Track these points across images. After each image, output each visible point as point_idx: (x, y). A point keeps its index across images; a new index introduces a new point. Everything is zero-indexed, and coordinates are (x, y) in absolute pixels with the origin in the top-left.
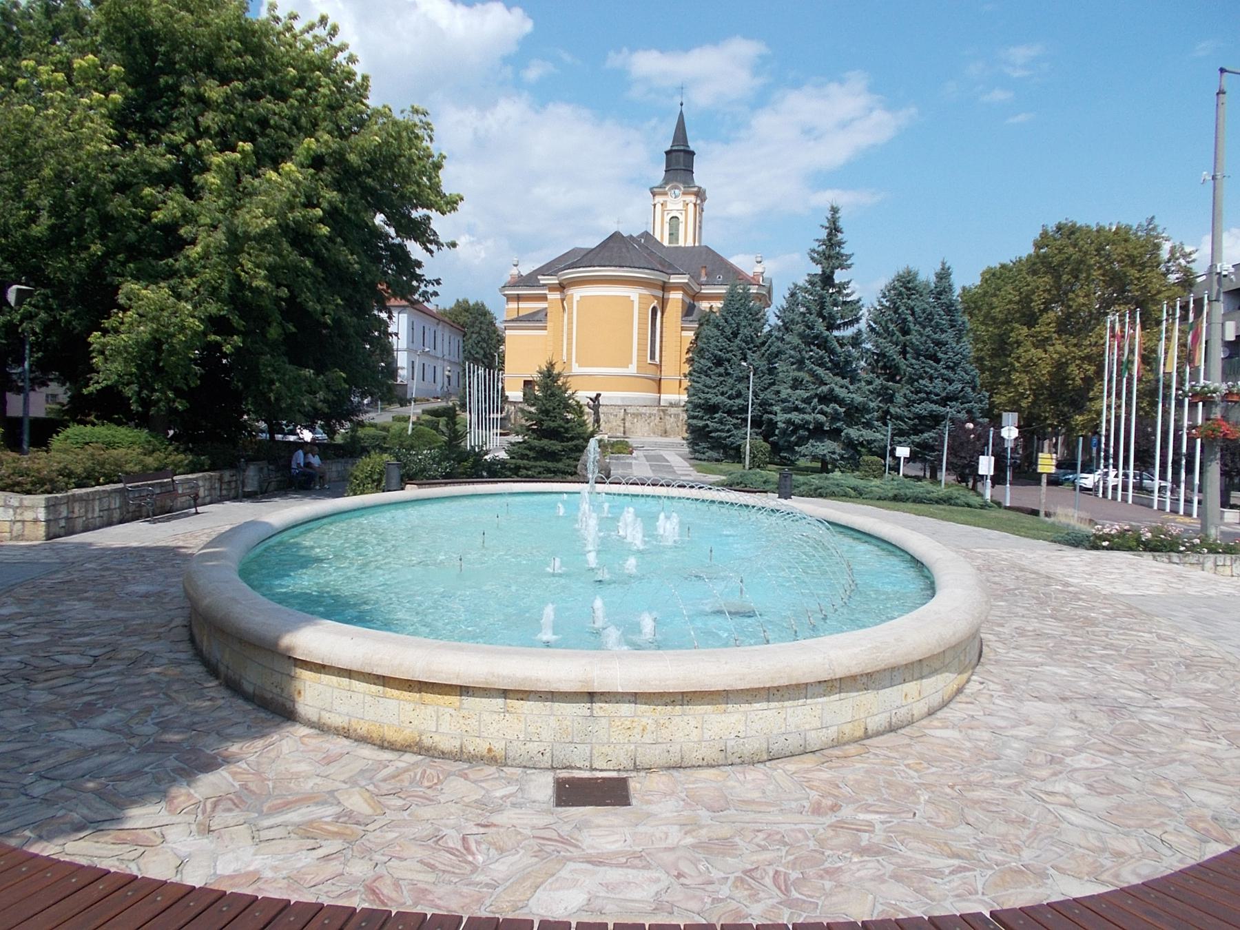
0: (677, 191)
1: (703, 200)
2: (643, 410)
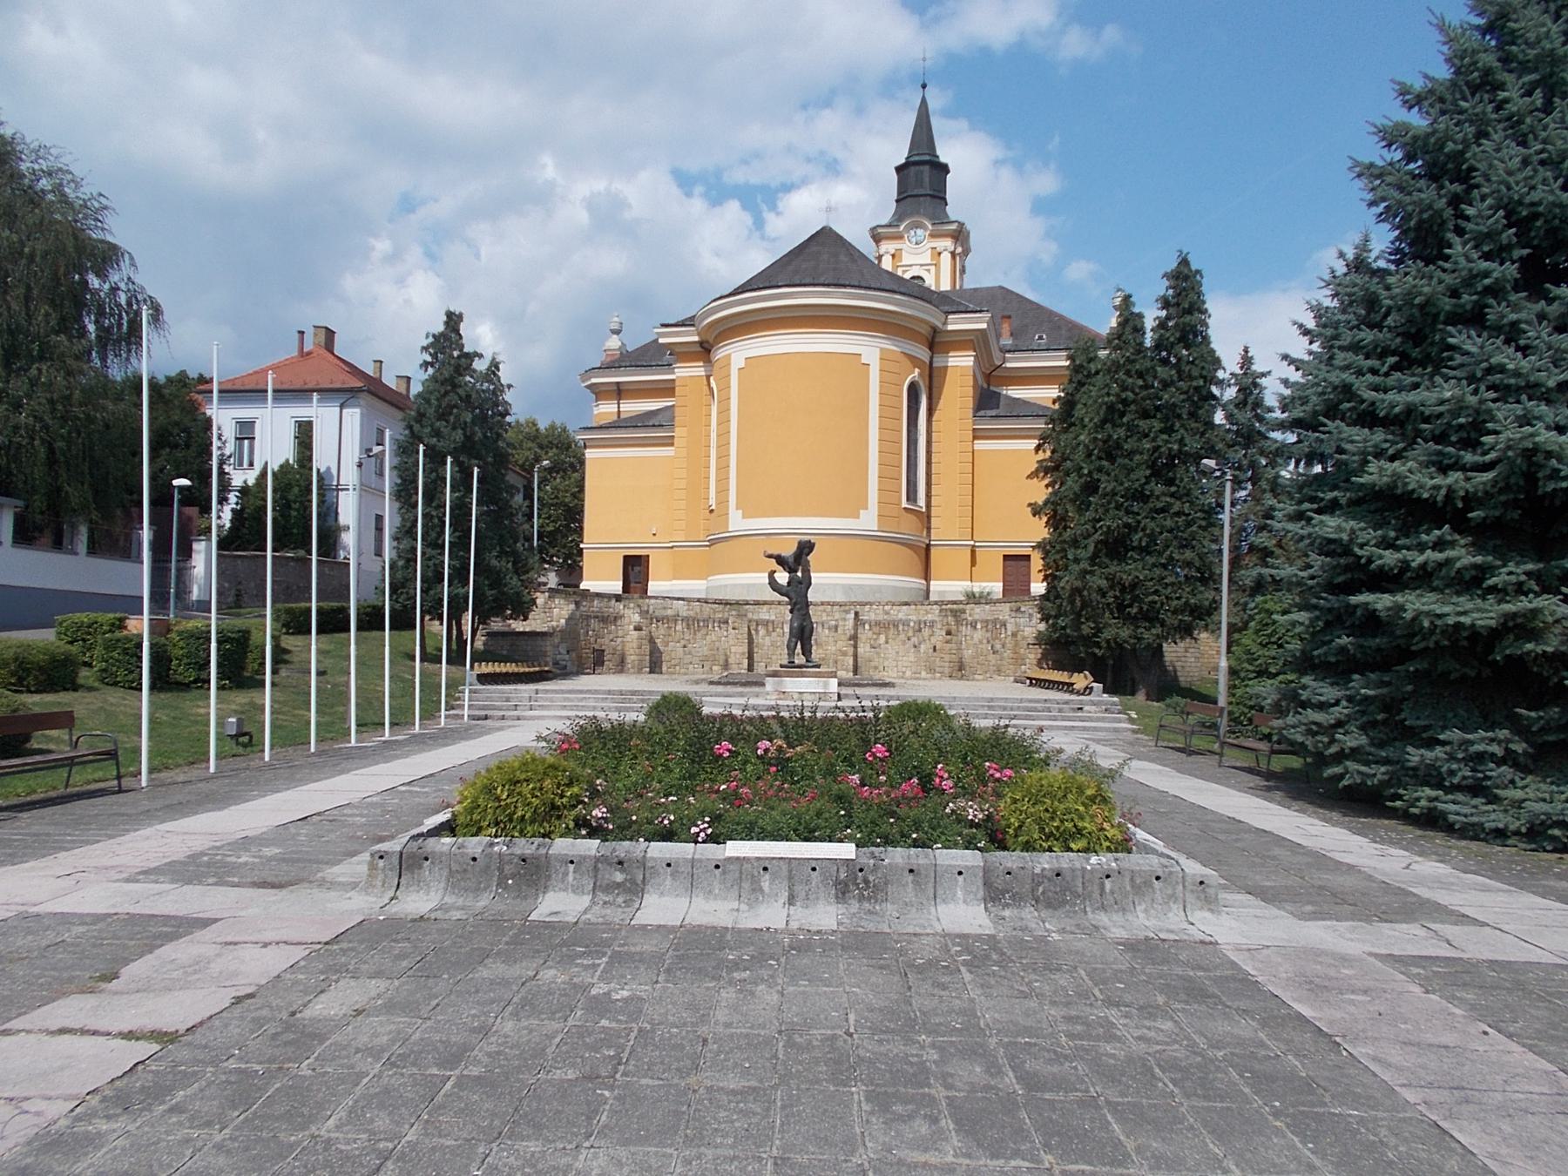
0: (920, 232)
1: (966, 252)
2: (902, 613)
